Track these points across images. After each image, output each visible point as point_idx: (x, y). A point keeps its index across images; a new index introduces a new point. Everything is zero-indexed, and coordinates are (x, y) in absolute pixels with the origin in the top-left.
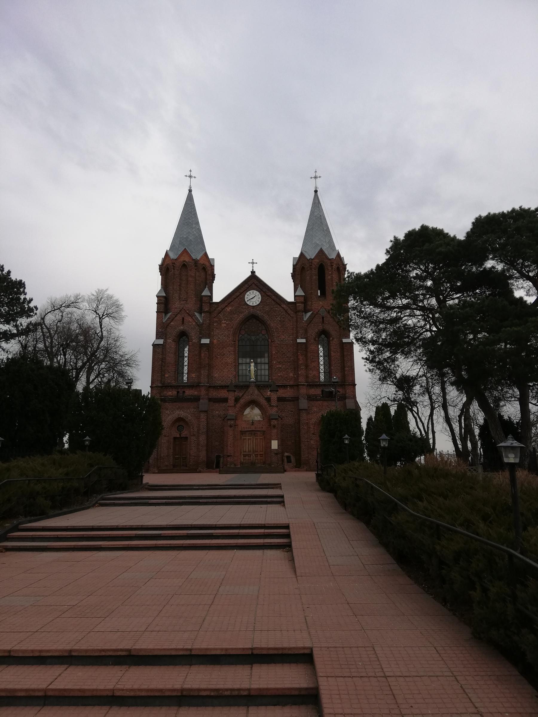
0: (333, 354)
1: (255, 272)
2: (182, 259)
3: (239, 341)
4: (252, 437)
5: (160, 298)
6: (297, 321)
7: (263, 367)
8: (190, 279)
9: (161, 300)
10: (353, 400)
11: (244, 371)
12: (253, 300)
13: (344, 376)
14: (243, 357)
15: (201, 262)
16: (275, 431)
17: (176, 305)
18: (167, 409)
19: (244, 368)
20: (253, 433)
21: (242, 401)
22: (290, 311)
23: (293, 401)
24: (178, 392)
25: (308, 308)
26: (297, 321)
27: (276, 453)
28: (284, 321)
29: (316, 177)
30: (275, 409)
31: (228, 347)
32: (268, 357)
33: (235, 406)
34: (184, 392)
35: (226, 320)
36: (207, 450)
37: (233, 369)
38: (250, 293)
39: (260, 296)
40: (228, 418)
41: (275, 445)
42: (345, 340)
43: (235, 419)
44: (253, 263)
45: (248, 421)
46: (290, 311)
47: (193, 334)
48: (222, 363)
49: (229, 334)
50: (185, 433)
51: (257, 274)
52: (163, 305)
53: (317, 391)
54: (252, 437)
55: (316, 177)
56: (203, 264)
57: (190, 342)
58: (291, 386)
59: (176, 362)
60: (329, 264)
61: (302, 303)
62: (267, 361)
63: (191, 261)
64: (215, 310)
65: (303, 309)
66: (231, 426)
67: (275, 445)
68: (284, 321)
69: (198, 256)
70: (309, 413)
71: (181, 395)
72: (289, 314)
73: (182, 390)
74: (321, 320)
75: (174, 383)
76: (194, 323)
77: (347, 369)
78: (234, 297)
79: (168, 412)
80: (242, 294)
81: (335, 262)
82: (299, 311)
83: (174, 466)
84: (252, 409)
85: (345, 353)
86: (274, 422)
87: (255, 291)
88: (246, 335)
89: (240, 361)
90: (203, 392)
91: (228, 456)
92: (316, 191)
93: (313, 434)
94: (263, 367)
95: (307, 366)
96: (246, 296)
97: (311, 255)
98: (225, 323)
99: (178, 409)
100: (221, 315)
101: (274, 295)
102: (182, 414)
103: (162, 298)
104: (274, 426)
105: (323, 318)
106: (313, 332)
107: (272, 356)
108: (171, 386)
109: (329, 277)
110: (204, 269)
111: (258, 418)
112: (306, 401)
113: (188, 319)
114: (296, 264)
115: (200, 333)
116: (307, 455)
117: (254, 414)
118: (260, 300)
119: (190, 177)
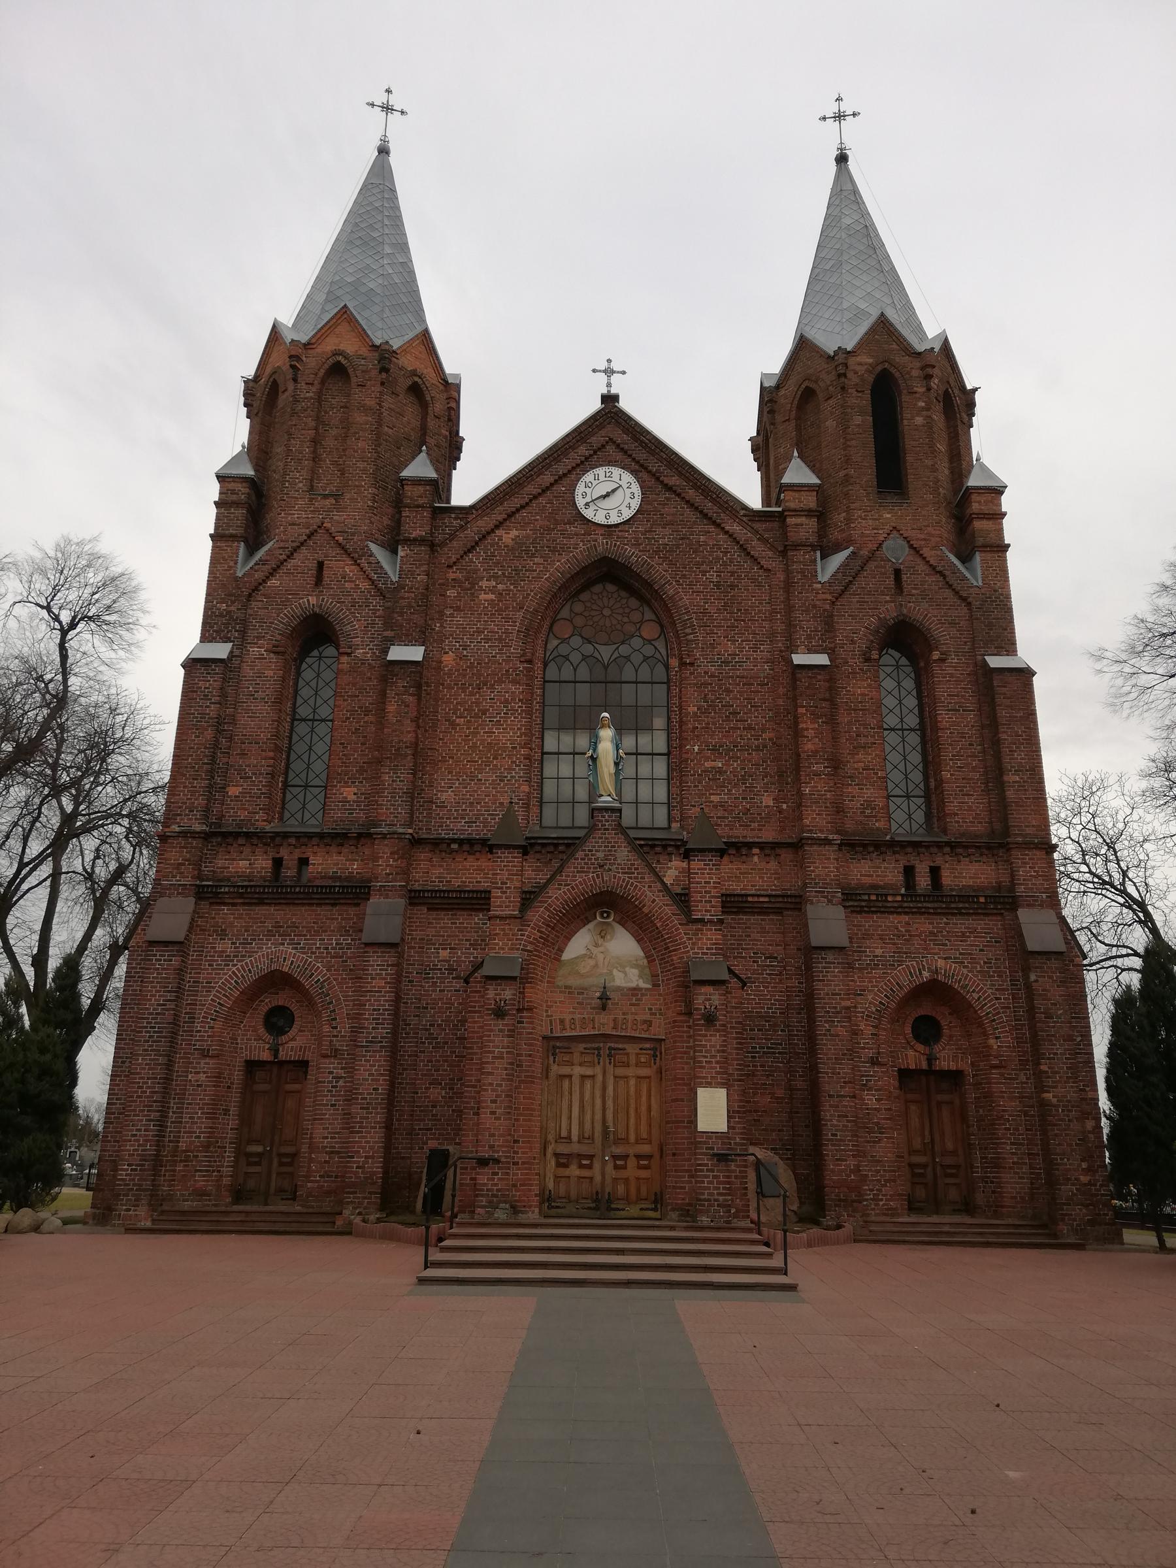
0: (944, 717)
1: (615, 398)
2: (329, 345)
3: (545, 665)
4: (598, 1070)
5: (232, 486)
6: (788, 585)
7: (645, 769)
8: (359, 418)
9: (233, 492)
10: (1050, 915)
11: (566, 787)
12: (609, 487)
13: (1001, 809)
14: (561, 728)
15: (407, 362)
16: (712, 1041)
17: (292, 515)
18: (223, 934)
19: (565, 770)
20: (604, 1046)
22: (757, 548)
23: (779, 911)
24: (278, 863)
25: (835, 535)
26: (788, 585)
27: (723, 1152)
28: (732, 587)
29: (839, 117)
30: (710, 937)
31: (500, 681)
32: (669, 730)
33: (521, 918)
34: (304, 862)
35: (495, 577)
36: (388, 1127)
37: (519, 772)
38: (596, 477)
39: (636, 488)
40: (486, 971)
41: (712, 1110)
42: (994, 662)
43: (522, 980)
44: (609, 372)
45: (582, 990)
46: (757, 548)
47: (358, 629)
48: (474, 747)
49: (506, 632)
50: (294, 1044)
51: (624, 404)
52: (240, 512)
53: (885, 872)
54: (598, 1070)
55: (839, 117)
56: (414, 373)
57: (344, 659)
58: (770, 849)
59: (277, 735)
60: (915, 373)
61: (809, 513)
62: (661, 745)
63: (364, 351)
64: (452, 537)
65: (813, 539)
66: (499, 1013)
67: (712, 1110)
68: (732, 587)
69: (387, 331)
70: (850, 966)
72: (755, 560)
73: (297, 854)
74: (890, 581)
75: (261, 822)
76: (364, 585)
77: (1011, 778)
78: (531, 489)
79: (226, 946)
80: (566, 481)
82: (796, 546)
83: (239, 1195)
84: (603, 933)
85: (1003, 714)
86: (707, 999)
87: (616, 472)
88: (576, 641)
89: (550, 744)
90: (385, 862)
91: (483, 1162)
92: (842, 159)
93: (874, 1062)
94: (645, 769)
95: (836, 764)
96: (580, 488)
97: (840, 335)
98: (492, 590)
99: (270, 934)
100: (476, 560)
101: (696, 487)
102: (286, 955)
103: (238, 487)
104: (710, 1019)
105: (897, 573)
106: (858, 625)
107: (681, 723)
108: (248, 835)
109: (919, 420)
110: (416, 390)
111: (630, 978)
112: (839, 912)
113: (340, 567)
114: (778, 387)
115: (388, 624)
116: (852, 1162)
117: (609, 956)
118: (636, 504)
119: (387, 108)
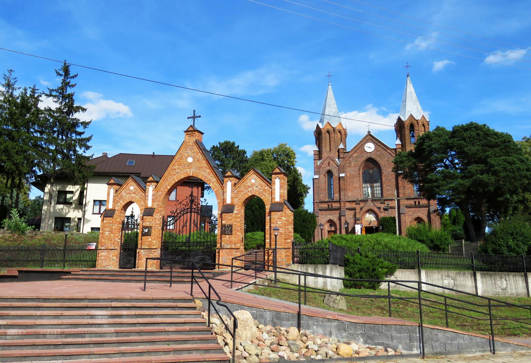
7: (377, 189)
21: (364, 210)
29: (407, 66)
71: (330, 206)
81: (421, 121)
100: (351, 159)
102: (332, 218)
113: (332, 162)
